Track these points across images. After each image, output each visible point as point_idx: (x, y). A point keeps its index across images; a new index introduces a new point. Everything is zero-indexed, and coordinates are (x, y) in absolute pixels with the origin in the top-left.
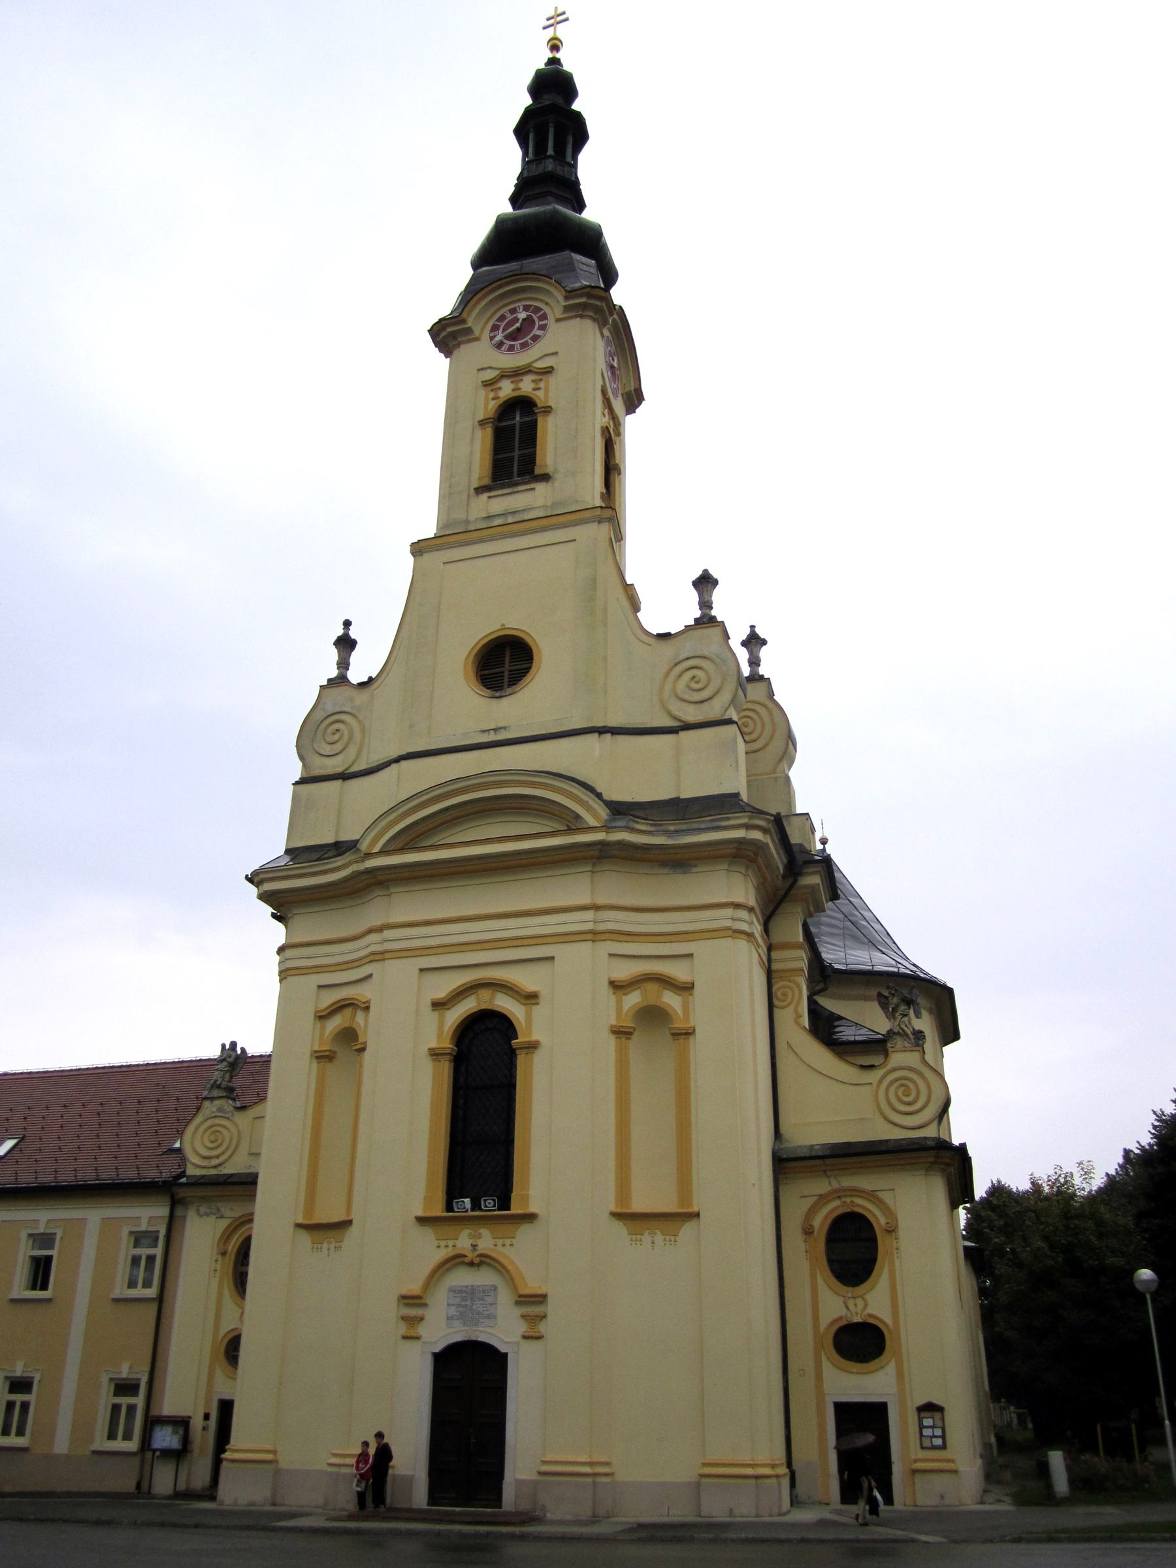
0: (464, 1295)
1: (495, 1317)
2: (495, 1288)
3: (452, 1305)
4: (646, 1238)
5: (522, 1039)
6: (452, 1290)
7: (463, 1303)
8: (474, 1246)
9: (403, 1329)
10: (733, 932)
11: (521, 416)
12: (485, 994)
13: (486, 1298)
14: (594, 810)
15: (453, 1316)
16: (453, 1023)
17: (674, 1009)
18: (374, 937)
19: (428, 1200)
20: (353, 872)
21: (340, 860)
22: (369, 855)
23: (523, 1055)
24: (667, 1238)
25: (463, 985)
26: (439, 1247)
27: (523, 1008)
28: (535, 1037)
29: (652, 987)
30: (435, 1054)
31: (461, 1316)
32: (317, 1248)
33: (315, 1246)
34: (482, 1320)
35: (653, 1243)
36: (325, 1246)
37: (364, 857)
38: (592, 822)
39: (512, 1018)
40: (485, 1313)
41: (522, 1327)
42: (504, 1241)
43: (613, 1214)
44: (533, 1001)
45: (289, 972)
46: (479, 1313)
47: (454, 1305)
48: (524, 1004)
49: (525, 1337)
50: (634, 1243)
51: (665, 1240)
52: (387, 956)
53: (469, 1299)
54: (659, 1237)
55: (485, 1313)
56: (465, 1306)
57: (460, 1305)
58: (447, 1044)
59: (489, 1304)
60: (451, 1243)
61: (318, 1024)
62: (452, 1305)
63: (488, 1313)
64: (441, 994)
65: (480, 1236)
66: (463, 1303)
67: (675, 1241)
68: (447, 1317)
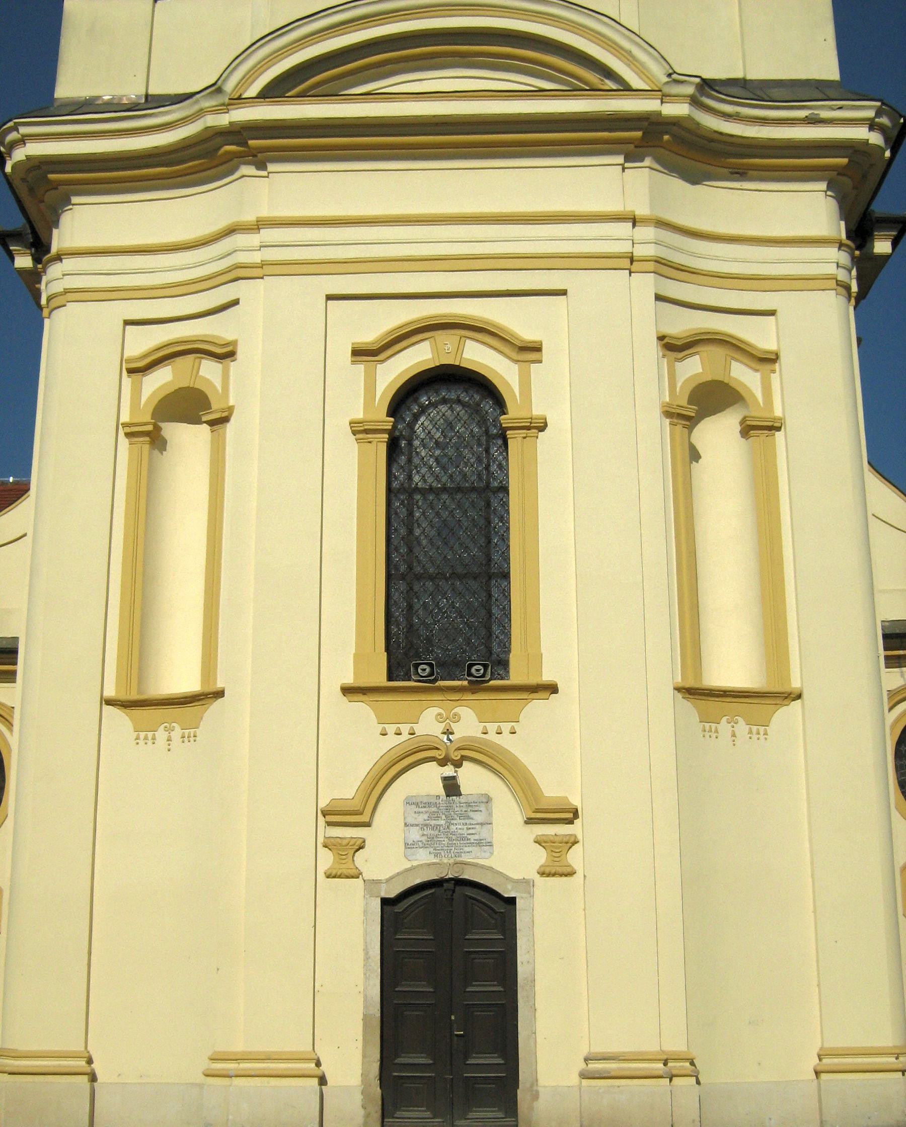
0: (434, 809)
1: (490, 844)
2: (488, 800)
3: (412, 825)
4: (724, 727)
5: (514, 412)
6: (410, 802)
7: (433, 823)
8: (448, 732)
9: (327, 859)
10: (838, 285)
11: (9, 480)
12: (448, 340)
13: (471, 814)
14: (642, 64)
15: (414, 843)
16: (406, 370)
17: (753, 396)
18: (240, 240)
19: (358, 658)
20: (207, 128)
21: (178, 109)
22: (238, 100)
23: (520, 439)
24: (754, 728)
25: (418, 320)
26: (384, 734)
27: (515, 368)
28: (537, 411)
29: (718, 352)
30: (360, 430)
31: (429, 843)
32: (146, 738)
33: (142, 735)
34: (467, 849)
35: (734, 735)
36: (161, 734)
37: (229, 105)
38: (636, 82)
39: (496, 381)
40: (472, 838)
41: (541, 857)
42: (499, 726)
43: (678, 689)
44: (533, 356)
45: (70, 296)
46: (463, 838)
47: (417, 825)
48: (516, 361)
49: (542, 874)
50: (707, 735)
51: (750, 732)
52: (268, 270)
53: (444, 817)
54: (742, 727)
55: (472, 838)
56: (437, 827)
57: (426, 825)
58: (381, 416)
59: (478, 824)
60: (405, 729)
61: (127, 381)
62: (412, 825)
63: (477, 837)
64: (370, 336)
65: (457, 718)
66: (433, 823)
67: (766, 734)
68: (406, 844)
